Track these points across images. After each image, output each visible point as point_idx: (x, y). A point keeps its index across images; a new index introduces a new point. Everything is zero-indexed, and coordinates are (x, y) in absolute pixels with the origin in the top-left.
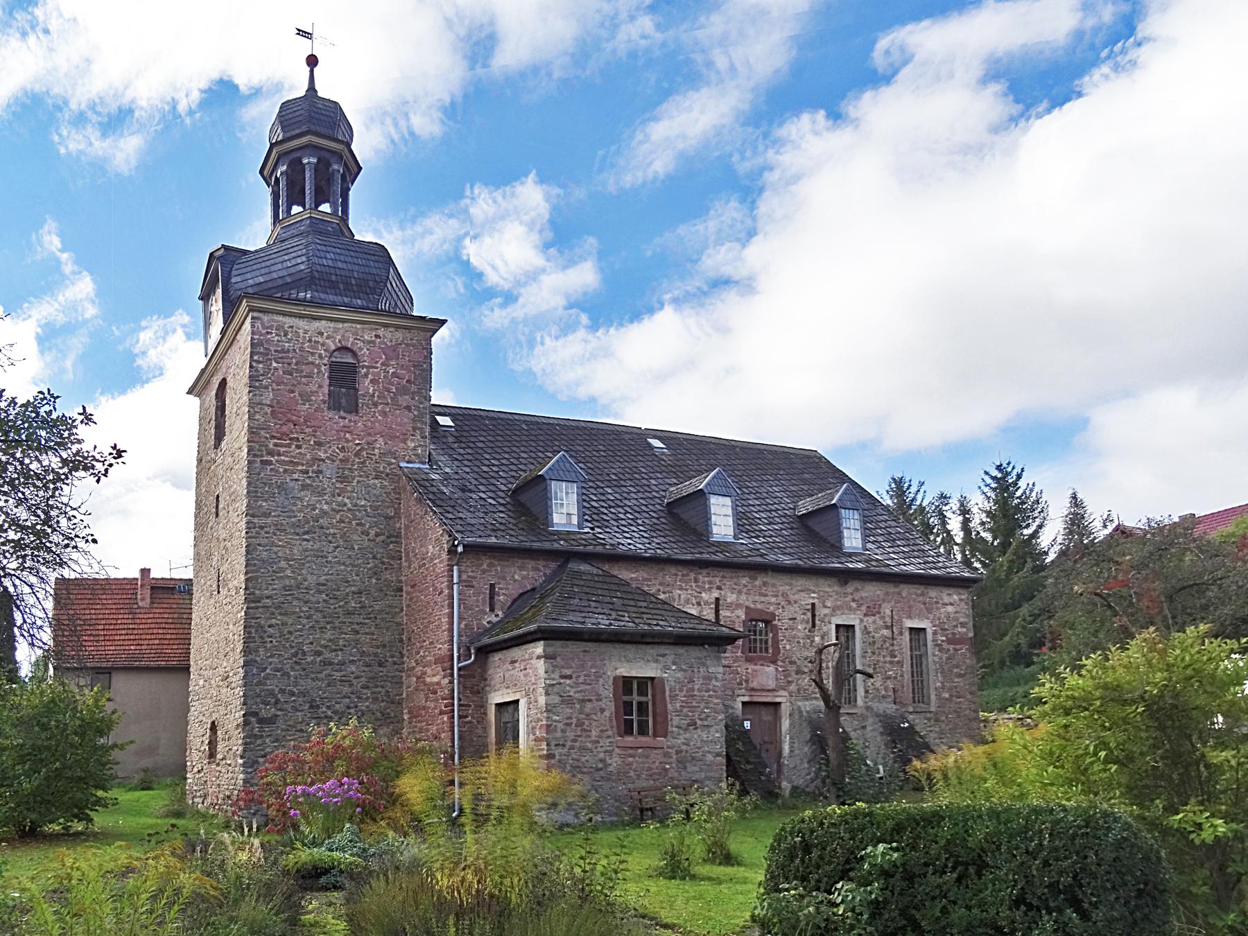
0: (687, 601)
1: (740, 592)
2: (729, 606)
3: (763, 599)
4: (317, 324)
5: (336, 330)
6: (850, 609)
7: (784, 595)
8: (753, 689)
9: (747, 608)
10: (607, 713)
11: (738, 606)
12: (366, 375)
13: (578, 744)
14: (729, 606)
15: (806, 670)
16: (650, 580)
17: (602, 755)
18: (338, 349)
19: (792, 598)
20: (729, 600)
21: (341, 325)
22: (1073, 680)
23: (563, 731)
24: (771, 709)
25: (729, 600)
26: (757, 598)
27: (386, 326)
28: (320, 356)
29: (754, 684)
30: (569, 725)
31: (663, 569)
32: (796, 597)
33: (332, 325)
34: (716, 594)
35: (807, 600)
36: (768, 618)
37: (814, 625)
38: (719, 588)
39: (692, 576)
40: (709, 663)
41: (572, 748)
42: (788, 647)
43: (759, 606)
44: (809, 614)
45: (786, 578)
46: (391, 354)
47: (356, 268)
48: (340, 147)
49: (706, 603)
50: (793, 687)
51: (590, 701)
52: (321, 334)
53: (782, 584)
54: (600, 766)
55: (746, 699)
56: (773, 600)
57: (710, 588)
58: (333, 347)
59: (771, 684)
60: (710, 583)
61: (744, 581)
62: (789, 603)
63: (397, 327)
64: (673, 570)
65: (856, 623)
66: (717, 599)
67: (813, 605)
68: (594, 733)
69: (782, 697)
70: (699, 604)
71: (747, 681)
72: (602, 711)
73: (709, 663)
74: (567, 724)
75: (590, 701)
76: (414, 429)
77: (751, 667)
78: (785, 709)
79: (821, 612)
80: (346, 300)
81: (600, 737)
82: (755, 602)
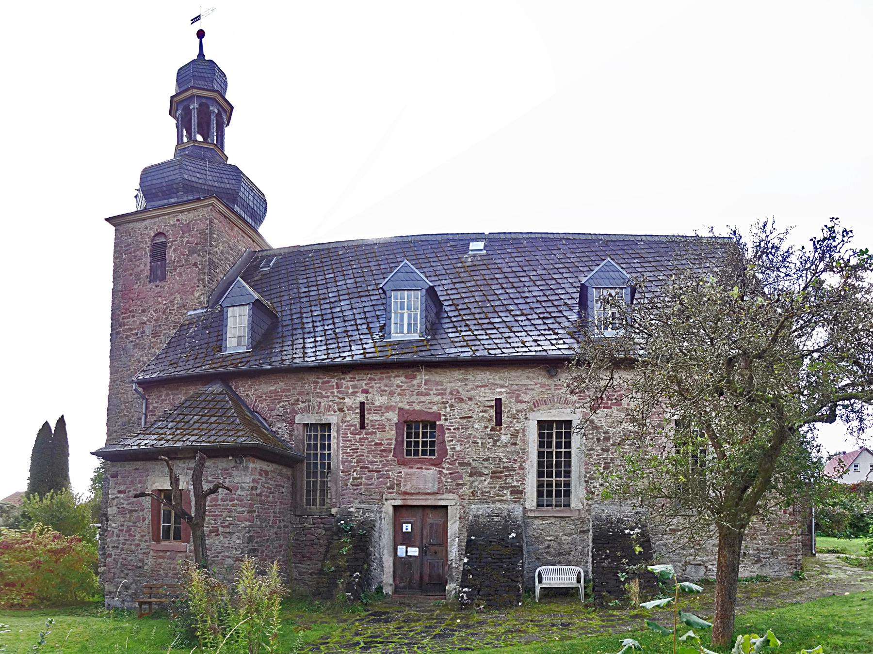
0: (328, 408)
1: (391, 394)
2: (378, 410)
3: (422, 398)
4: (145, 223)
5: (155, 223)
6: (566, 402)
7: (455, 393)
8: (406, 493)
9: (401, 409)
10: (146, 522)
11: (389, 408)
12: (171, 247)
13: (126, 547)
14: (378, 410)
15: (486, 472)
16: (289, 391)
17: (141, 556)
18: (156, 235)
19: (463, 394)
20: (377, 403)
21: (157, 220)
22: (344, 551)
23: (118, 536)
24: (444, 510)
25: (377, 403)
26: (413, 398)
27: (182, 212)
28: (146, 243)
29: (408, 488)
30: (121, 530)
31: (303, 379)
32: (469, 394)
33: (152, 221)
34: (361, 398)
35: (488, 396)
36: (428, 418)
37: (499, 423)
38: (366, 392)
39: (334, 381)
40: (234, 473)
41: (122, 550)
42: (458, 448)
43: (417, 407)
44: (493, 412)
45: (457, 374)
46: (186, 229)
47: (163, 180)
48: (214, 95)
49: (350, 408)
50: (466, 490)
51: (136, 511)
52: (146, 228)
53: (452, 380)
54: (140, 564)
55: (399, 502)
56: (438, 399)
57: (354, 393)
58: (153, 235)
59: (432, 487)
60: (354, 387)
61: (398, 381)
62: (462, 400)
63: (189, 210)
64: (313, 378)
65: (576, 419)
66: (362, 404)
67: (498, 402)
68: (137, 537)
69: (448, 500)
70: (341, 410)
71: (399, 485)
72: (144, 519)
73: (234, 473)
74: (120, 530)
75: (136, 511)
76: (199, 280)
77: (404, 470)
78: (454, 513)
79: (510, 407)
80: (166, 201)
81: (140, 541)
82: (410, 403)
